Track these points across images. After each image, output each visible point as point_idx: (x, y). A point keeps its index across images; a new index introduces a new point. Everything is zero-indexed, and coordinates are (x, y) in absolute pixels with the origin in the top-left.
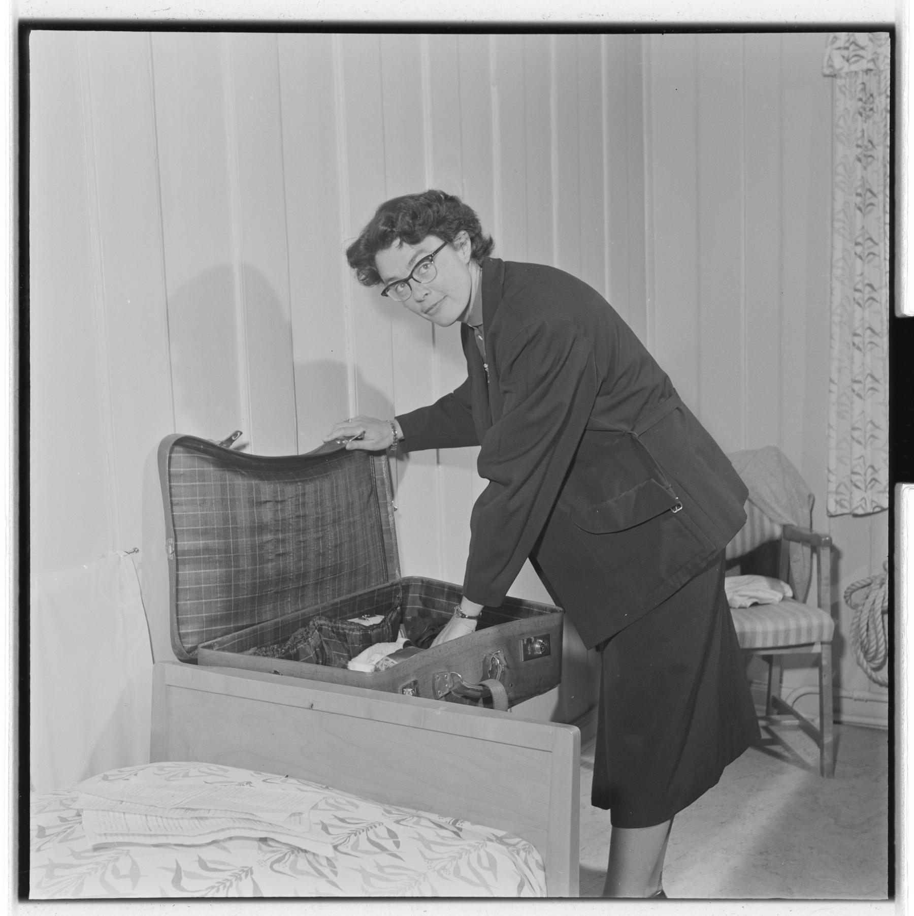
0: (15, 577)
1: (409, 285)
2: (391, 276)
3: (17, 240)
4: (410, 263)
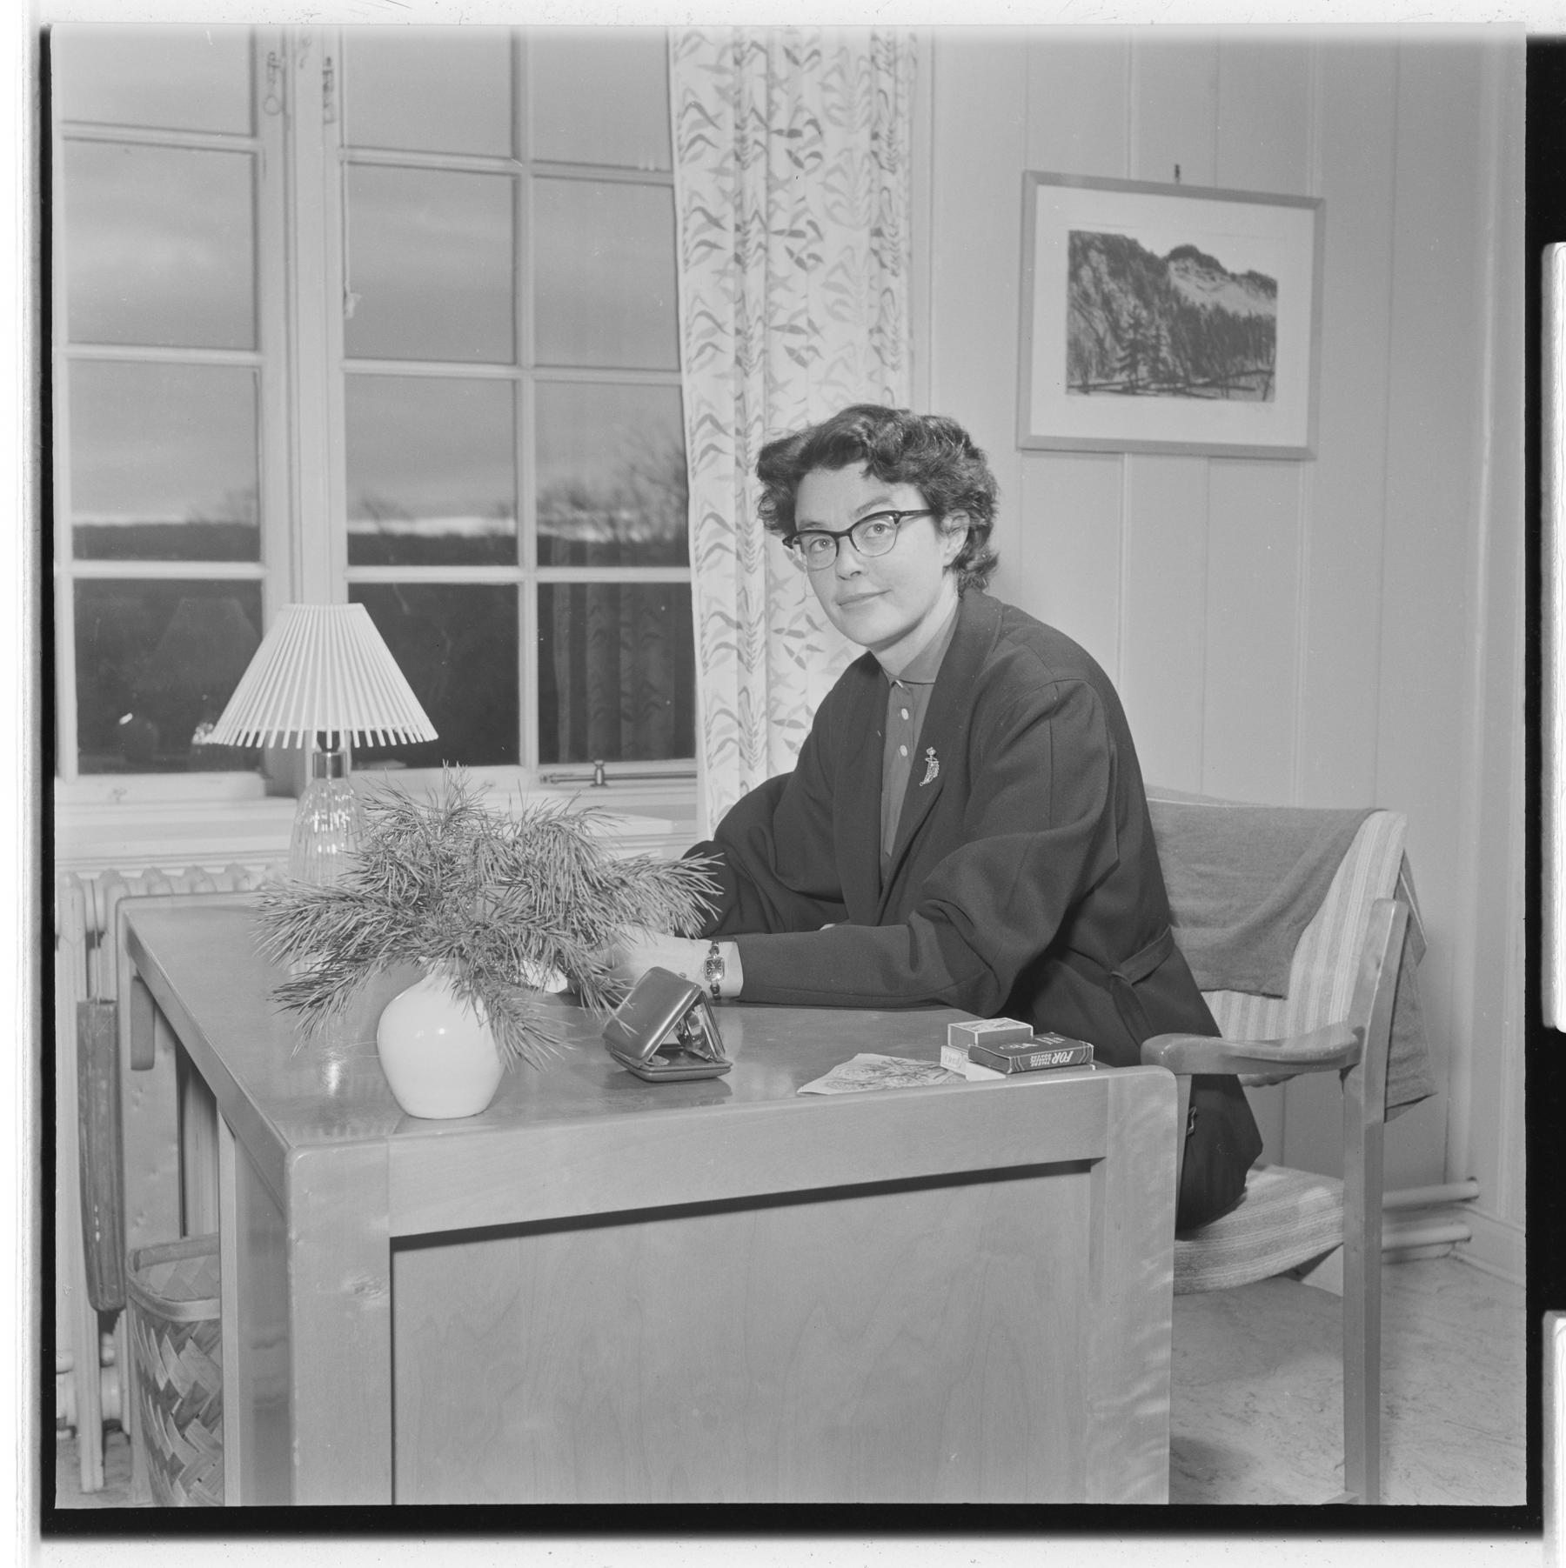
0: (34, 619)
1: (838, 545)
2: (816, 519)
3: (39, 527)
4: (859, 510)
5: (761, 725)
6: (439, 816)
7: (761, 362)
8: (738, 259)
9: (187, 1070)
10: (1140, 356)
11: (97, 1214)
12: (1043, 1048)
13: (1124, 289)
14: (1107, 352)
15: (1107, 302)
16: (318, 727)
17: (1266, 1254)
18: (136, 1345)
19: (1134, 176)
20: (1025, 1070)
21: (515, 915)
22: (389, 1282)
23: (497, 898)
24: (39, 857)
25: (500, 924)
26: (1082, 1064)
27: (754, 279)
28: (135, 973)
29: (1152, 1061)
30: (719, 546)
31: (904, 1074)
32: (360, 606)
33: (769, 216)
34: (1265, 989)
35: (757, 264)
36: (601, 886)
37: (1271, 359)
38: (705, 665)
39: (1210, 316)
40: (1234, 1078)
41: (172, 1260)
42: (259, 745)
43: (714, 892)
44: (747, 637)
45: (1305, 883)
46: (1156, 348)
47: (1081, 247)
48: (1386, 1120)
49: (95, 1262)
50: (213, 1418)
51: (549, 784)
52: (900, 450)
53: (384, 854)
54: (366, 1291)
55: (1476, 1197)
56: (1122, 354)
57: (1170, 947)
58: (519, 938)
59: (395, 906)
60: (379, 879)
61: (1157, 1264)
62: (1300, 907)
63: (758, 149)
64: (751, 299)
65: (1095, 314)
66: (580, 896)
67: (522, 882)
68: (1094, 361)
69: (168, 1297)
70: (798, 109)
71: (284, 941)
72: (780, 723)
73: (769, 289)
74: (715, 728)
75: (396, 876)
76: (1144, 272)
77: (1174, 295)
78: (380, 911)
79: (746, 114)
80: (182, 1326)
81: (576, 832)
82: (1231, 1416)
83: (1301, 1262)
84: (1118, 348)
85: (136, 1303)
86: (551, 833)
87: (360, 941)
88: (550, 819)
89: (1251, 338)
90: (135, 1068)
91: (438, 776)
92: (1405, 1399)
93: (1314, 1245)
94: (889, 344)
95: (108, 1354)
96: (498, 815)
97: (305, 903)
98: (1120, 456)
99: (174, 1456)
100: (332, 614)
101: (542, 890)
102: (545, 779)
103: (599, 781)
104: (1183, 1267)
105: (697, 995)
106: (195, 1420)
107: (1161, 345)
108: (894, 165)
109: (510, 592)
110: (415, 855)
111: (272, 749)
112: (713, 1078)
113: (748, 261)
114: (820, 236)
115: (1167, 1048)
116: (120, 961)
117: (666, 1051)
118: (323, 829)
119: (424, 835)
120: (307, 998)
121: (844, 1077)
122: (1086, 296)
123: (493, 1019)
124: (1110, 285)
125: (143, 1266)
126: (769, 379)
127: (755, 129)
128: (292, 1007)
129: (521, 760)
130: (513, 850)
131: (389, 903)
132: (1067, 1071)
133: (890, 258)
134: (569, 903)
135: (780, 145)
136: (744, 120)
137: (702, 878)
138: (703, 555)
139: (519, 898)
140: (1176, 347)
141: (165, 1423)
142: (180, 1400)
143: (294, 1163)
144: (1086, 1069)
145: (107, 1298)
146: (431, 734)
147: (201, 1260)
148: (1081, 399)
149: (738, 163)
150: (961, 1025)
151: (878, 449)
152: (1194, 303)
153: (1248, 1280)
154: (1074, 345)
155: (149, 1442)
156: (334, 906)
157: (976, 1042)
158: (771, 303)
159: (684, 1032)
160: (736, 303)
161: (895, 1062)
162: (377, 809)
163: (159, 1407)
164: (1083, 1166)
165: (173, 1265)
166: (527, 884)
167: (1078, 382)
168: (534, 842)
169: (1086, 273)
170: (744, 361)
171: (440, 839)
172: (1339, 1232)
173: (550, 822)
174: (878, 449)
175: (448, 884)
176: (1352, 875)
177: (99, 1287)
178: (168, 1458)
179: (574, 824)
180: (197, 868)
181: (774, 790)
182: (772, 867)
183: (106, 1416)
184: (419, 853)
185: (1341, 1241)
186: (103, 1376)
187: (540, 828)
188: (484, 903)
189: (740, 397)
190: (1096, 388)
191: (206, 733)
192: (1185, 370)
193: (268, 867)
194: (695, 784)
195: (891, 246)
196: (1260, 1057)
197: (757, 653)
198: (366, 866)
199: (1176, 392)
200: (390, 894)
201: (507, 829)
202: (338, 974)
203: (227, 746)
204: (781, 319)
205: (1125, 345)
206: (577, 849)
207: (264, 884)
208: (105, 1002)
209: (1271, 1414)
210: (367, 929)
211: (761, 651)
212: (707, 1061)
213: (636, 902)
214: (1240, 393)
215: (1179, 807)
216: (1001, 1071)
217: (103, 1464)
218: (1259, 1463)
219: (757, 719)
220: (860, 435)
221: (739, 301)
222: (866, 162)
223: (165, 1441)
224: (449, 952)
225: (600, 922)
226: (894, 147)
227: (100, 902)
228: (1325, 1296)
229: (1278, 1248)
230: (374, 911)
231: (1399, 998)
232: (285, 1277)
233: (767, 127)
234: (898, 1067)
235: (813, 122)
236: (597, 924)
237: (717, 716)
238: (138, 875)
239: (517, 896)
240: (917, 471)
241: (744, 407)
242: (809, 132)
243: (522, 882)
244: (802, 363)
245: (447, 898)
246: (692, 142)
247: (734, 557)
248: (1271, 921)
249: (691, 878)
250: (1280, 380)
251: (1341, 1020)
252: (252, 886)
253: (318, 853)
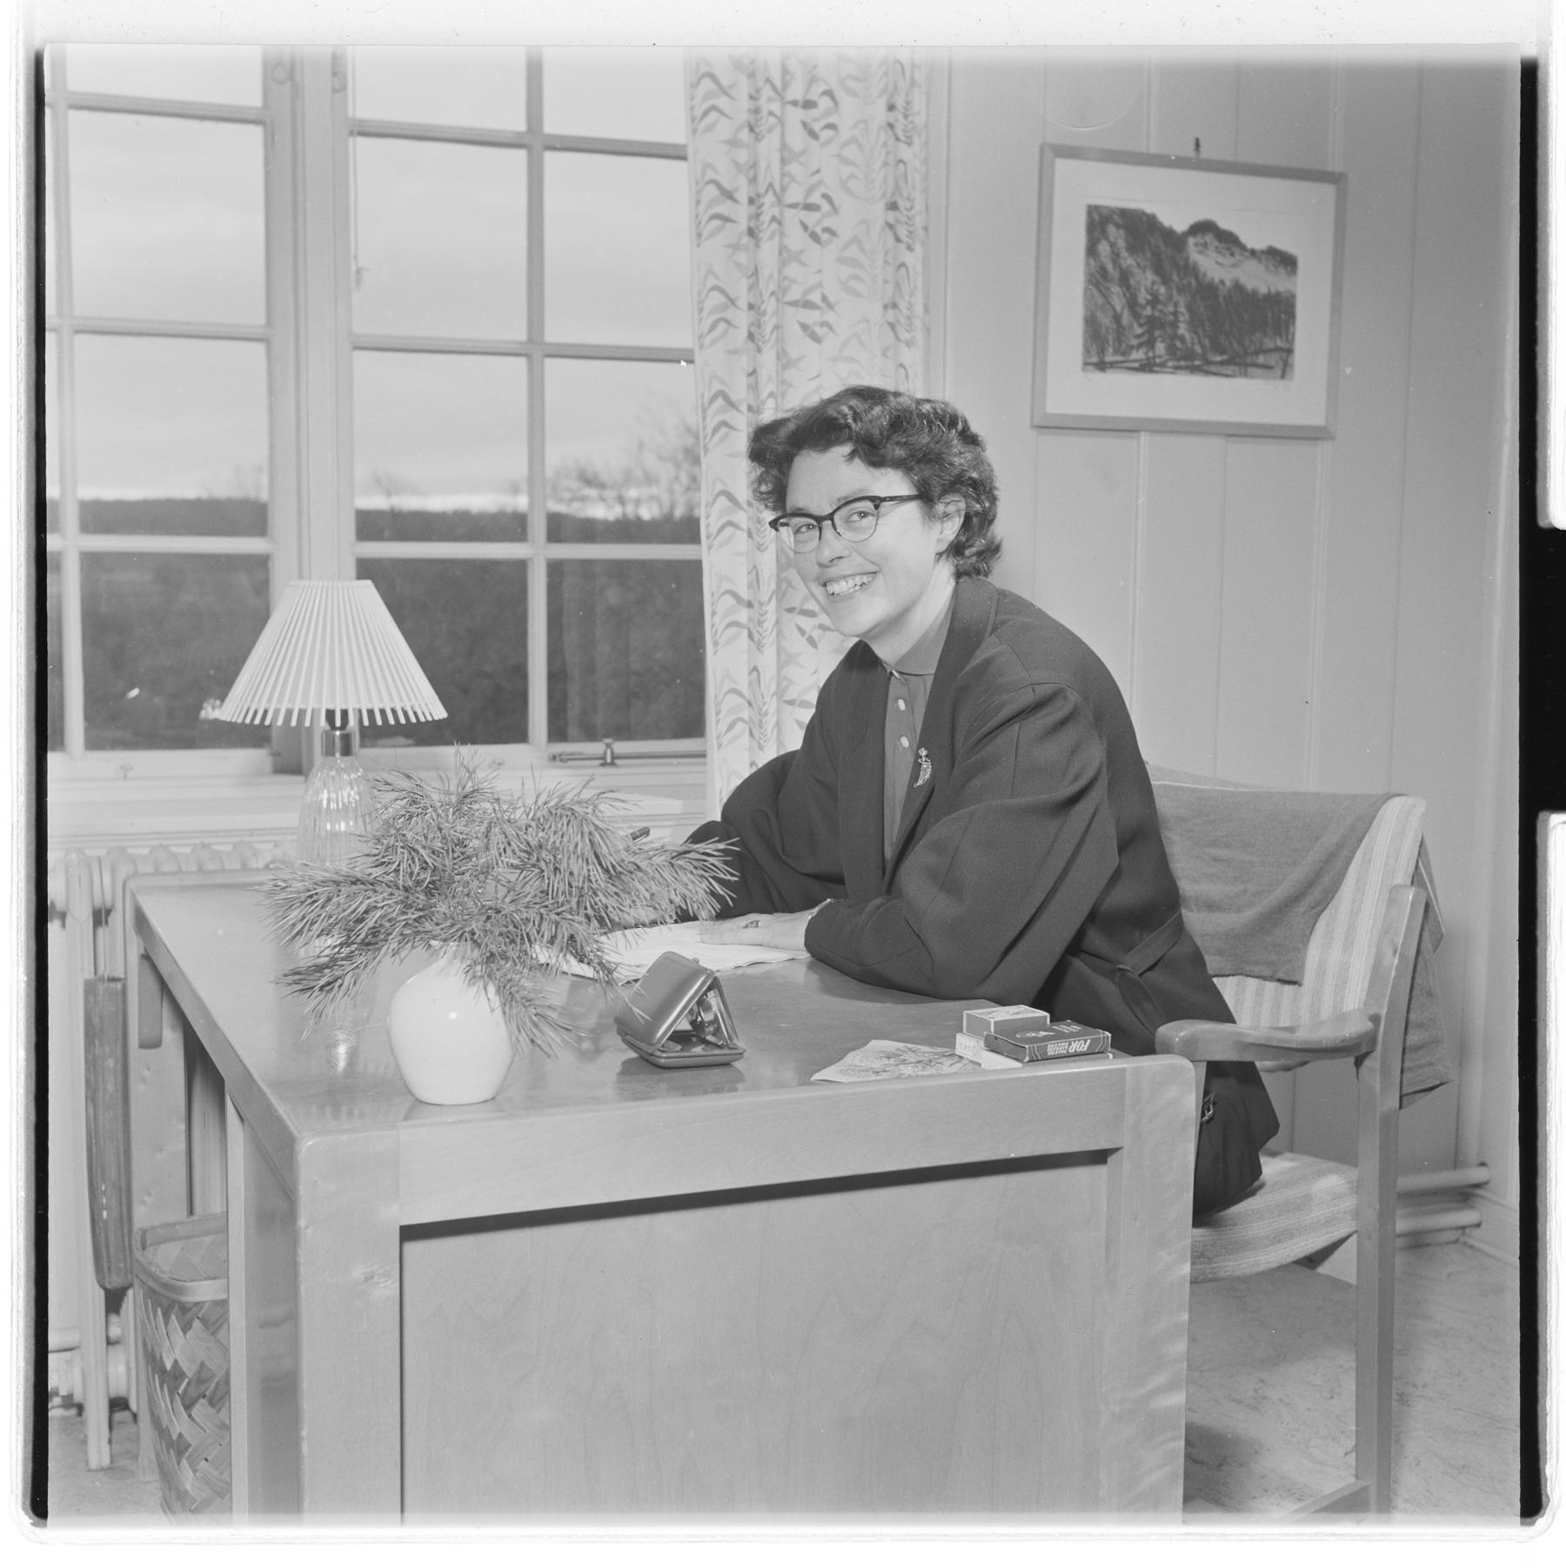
0: (28, 503)
5: (772, 705)
6: (449, 799)
7: (774, 337)
8: (751, 232)
9: (198, 1060)
10: (1157, 333)
11: (104, 1193)
12: (1060, 1036)
13: (1142, 264)
14: (1124, 329)
15: (1125, 277)
16: (326, 705)
17: (1279, 1242)
18: (143, 1323)
19: (1153, 150)
20: (1041, 1058)
21: (528, 899)
22: (398, 1271)
23: (509, 882)
24: (33, 645)
25: (512, 909)
26: (1099, 1053)
27: (768, 253)
28: (142, 951)
29: (1168, 1049)
30: (730, 524)
31: (919, 1062)
32: (369, 582)
33: (783, 189)
34: (1280, 975)
35: (771, 237)
36: (615, 871)
37: (1290, 337)
38: (716, 643)
39: (1229, 292)
40: (1251, 1065)
41: (180, 1239)
42: (267, 722)
43: (729, 877)
44: (758, 616)
45: (1321, 868)
46: (1174, 325)
47: (1099, 222)
48: (1401, 1107)
49: (102, 1239)
50: (219, 1398)
51: (558, 763)
52: (885, 434)
53: (396, 837)
54: (375, 1279)
55: (1486, 1183)
56: (1139, 331)
57: (1180, 926)
58: (532, 923)
59: (406, 889)
60: (389, 863)
61: (1173, 1256)
62: (1316, 893)
63: (772, 120)
64: (765, 273)
65: (1113, 290)
66: (593, 880)
67: (534, 866)
68: (1111, 338)
69: (175, 1276)
70: (813, 80)
71: (294, 925)
72: (791, 703)
73: (783, 263)
74: (724, 708)
75: (408, 860)
76: (1163, 248)
77: (1193, 271)
78: (391, 894)
79: (761, 84)
80: (189, 1306)
81: (589, 815)
82: (1240, 1402)
83: (1315, 1250)
84: (1135, 325)
85: (144, 1283)
86: (564, 818)
87: (371, 924)
88: (563, 802)
89: (1270, 315)
90: (142, 1046)
91: (449, 754)
92: (1415, 1385)
93: (1328, 1233)
94: (903, 320)
95: (115, 1331)
96: (511, 798)
97: (316, 886)
98: (1136, 434)
99: (180, 1435)
100: (340, 591)
101: (555, 874)
102: (554, 758)
103: (609, 760)
104: (1198, 1256)
105: (710, 982)
106: (202, 1401)
107: (1179, 321)
108: (909, 137)
109: (520, 568)
110: (426, 838)
111: (280, 727)
112: (727, 1064)
113: (761, 235)
114: (835, 209)
115: (1182, 1034)
116: (128, 937)
117: (679, 1037)
118: (332, 807)
119: (435, 817)
120: (318, 982)
121: (858, 1064)
122: (1103, 272)
123: (505, 1004)
124: (1128, 261)
125: (151, 1245)
126: (782, 355)
127: (770, 99)
128: (302, 990)
129: (531, 740)
130: (525, 833)
131: (401, 887)
132: (1086, 1060)
133: (905, 232)
134: (582, 888)
135: (795, 115)
136: (758, 91)
137: (717, 863)
138: (714, 533)
139: (531, 882)
140: (1193, 325)
141: (172, 1402)
142: (186, 1381)
143: (304, 1150)
144: (1104, 1058)
145: (114, 1276)
146: (440, 713)
147: (208, 1239)
148: (1098, 376)
149: (752, 135)
150: (977, 1012)
151: (862, 432)
152: (1213, 279)
153: (1261, 1268)
154: (1091, 322)
155: (156, 1421)
156: (345, 890)
157: (992, 1030)
158: (785, 278)
159: (697, 1018)
160: (749, 277)
161: (910, 1049)
162: (387, 791)
163: (165, 1386)
164: (1099, 1157)
165: (179, 1244)
166: (540, 868)
167: (1095, 359)
168: (547, 827)
169: (1104, 248)
170: (757, 336)
171: (451, 821)
172: (1352, 1220)
173: (563, 805)
174: (862, 432)
175: (460, 867)
176: (1370, 861)
177: (106, 1265)
178: (175, 1437)
179: (587, 807)
180: (204, 846)
181: (777, 773)
182: (779, 849)
183: (113, 1394)
184: (430, 836)
185: (1354, 1229)
186: (110, 1354)
187: (554, 812)
188: (496, 887)
189: (753, 373)
190: (1112, 365)
191: (213, 708)
192: (1202, 347)
193: (276, 845)
194: (705, 764)
195: (906, 219)
196: (1275, 1044)
197: (768, 632)
198: (377, 849)
199: (1193, 370)
200: (401, 878)
201: (519, 813)
202: (348, 957)
203: (236, 723)
204: (795, 294)
205: (1142, 321)
206: (590, 833)
207: (272, 862)
208: (113, 980)
209: (1281, 1400)
210: (379, 913)
211: (772, 630)
212: (720, 1047)
213: (651, 888)
214: (1259, 371)
215: (1193, 791)
216: (1017, 1060)
217: (110, 1442)
218: (1269, 1450)
219: (767, 699)
220: (845, 416)
221: (752, 275)
222: (882, 134)
223: (171, 1421)
224: (461, 937)
225: (613, 908)
226: (910, 119)
227: (107, 880)
228: (1335, 1283)
229: (1292, 1236)
230: (385, 895)
231: (1415, 985)
232: (295, 1265)
233: (782, 98)
234: (912, 1054)
235: (829, 93)
236: (610, 909)
237: (728, 695)
238: (145, 852)
239: (530, 880)
240: (904, 456)
241: (757, 383)
242: (824, 103)
243: (534, 866)
244: (816, 339)
245: (459, 882)
246: (706, 113)
247: (745, 535)
248: (1287, 906)
249: (705, 863)
250: (1299, 358)
251: (1357, 1007)
252: (261, 864)
253: (327, 831)
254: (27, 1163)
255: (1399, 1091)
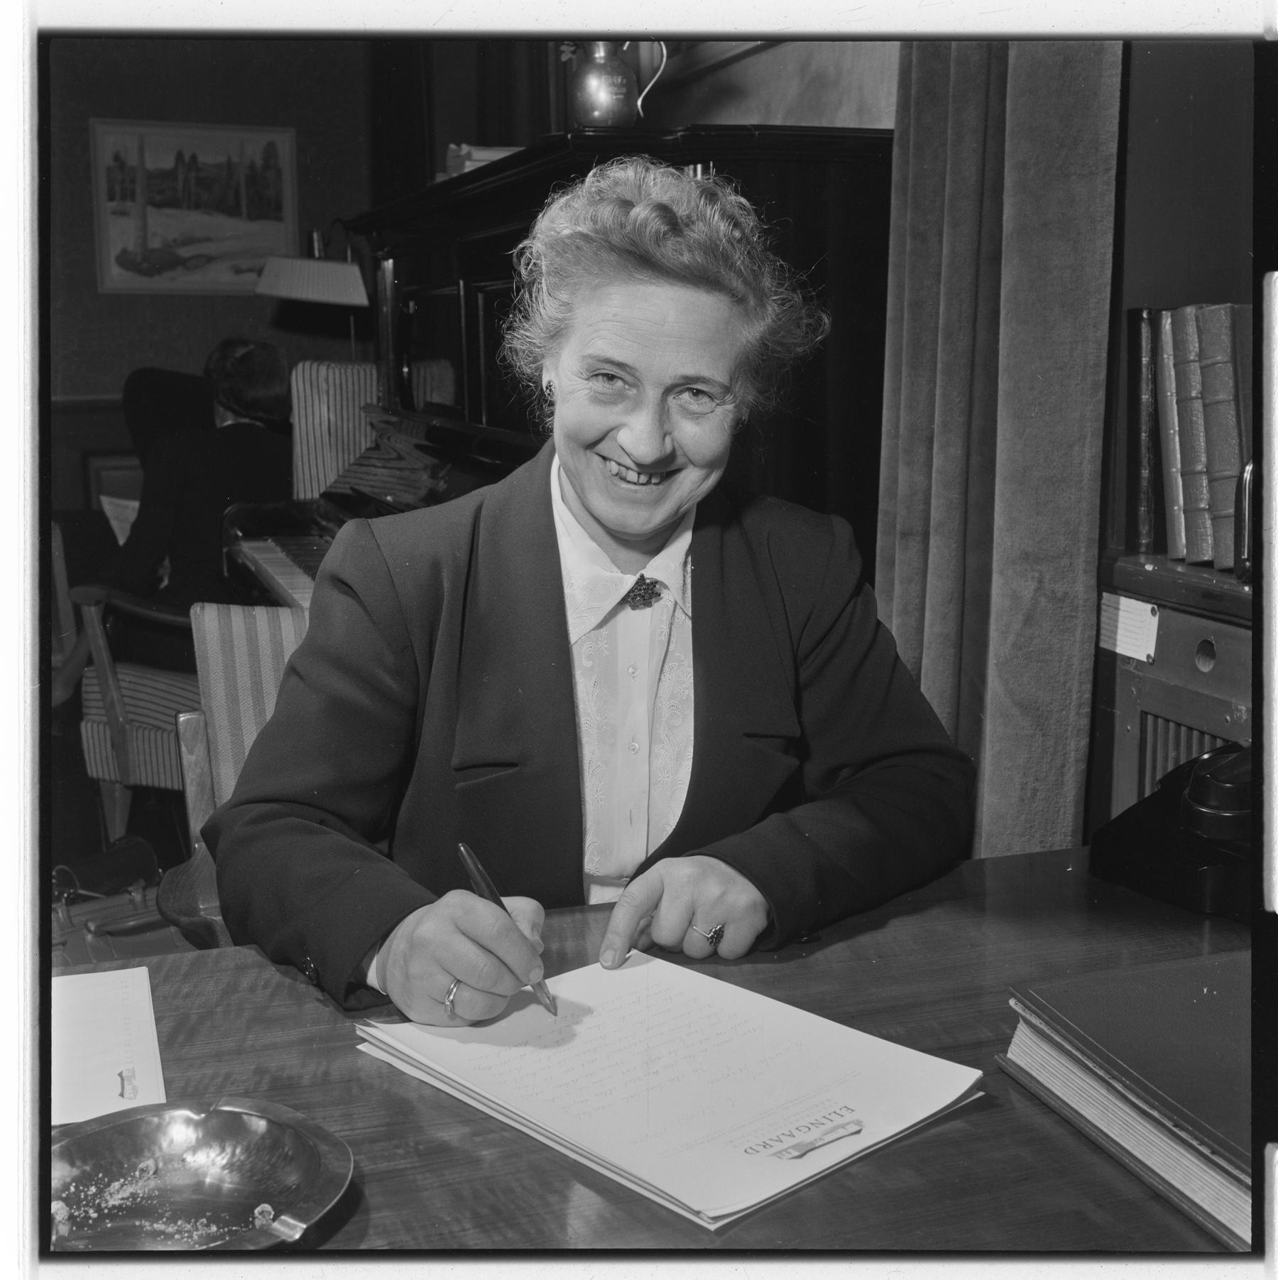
0: (32, 199)
248: (478, 513)
254: (33, 969)
255: (416, 512)
